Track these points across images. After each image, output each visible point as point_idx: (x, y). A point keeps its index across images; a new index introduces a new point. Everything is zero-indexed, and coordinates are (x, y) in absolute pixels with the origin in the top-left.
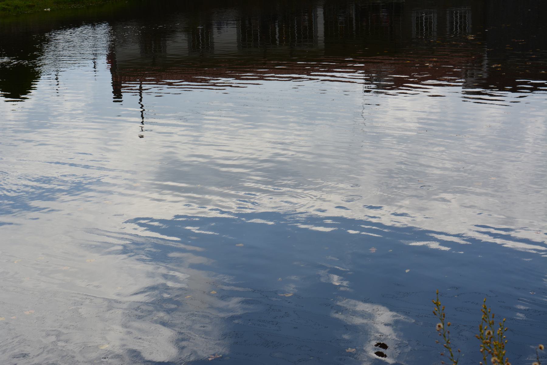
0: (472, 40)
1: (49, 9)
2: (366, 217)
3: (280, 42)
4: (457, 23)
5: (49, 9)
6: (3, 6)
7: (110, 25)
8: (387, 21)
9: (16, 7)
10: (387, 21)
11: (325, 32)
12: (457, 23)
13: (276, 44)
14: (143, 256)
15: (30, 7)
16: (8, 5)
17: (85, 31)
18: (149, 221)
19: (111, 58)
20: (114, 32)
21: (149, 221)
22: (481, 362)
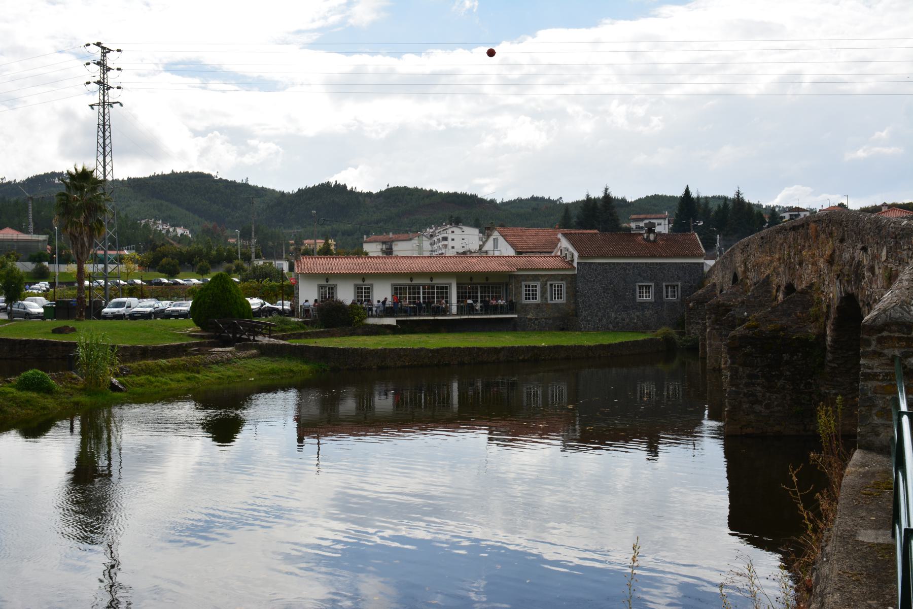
0: (571, 409)
1: (253, 379)
2: (422, 486)
3: (424, 407)
4: (556, 396)
5: (253, 379)
6: (219, 376)
7: (298, 391)
8: (476, 203)
9: (229, 377)
10: (476, 203)
11: (458, 402)
12: (556, 396)
13: (421, 407)
14: (628, 568)
15: (239, 377)
16: (223, 375)
17: (280, 395)
18: (697, 588)
19: (298, 419)
20: (300, 397)
21: (697, 588)
22: (528, 580)
